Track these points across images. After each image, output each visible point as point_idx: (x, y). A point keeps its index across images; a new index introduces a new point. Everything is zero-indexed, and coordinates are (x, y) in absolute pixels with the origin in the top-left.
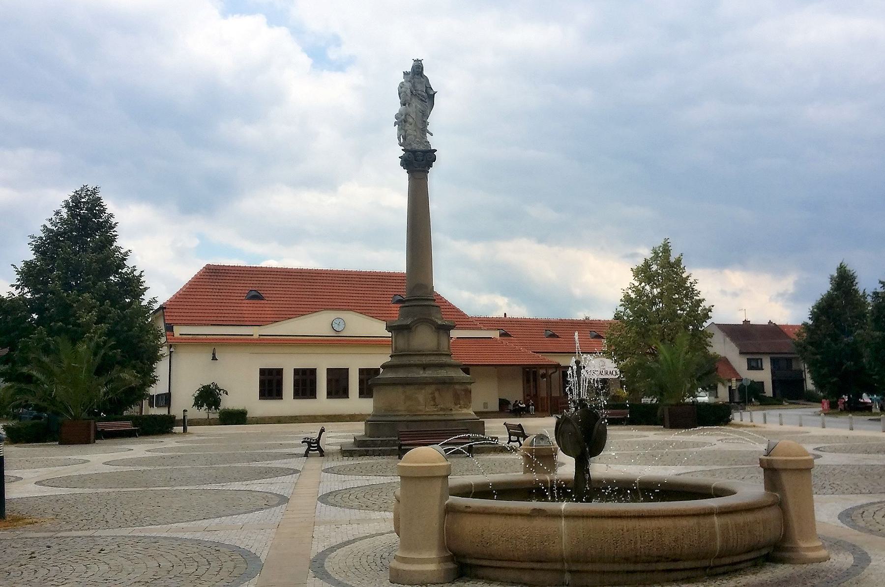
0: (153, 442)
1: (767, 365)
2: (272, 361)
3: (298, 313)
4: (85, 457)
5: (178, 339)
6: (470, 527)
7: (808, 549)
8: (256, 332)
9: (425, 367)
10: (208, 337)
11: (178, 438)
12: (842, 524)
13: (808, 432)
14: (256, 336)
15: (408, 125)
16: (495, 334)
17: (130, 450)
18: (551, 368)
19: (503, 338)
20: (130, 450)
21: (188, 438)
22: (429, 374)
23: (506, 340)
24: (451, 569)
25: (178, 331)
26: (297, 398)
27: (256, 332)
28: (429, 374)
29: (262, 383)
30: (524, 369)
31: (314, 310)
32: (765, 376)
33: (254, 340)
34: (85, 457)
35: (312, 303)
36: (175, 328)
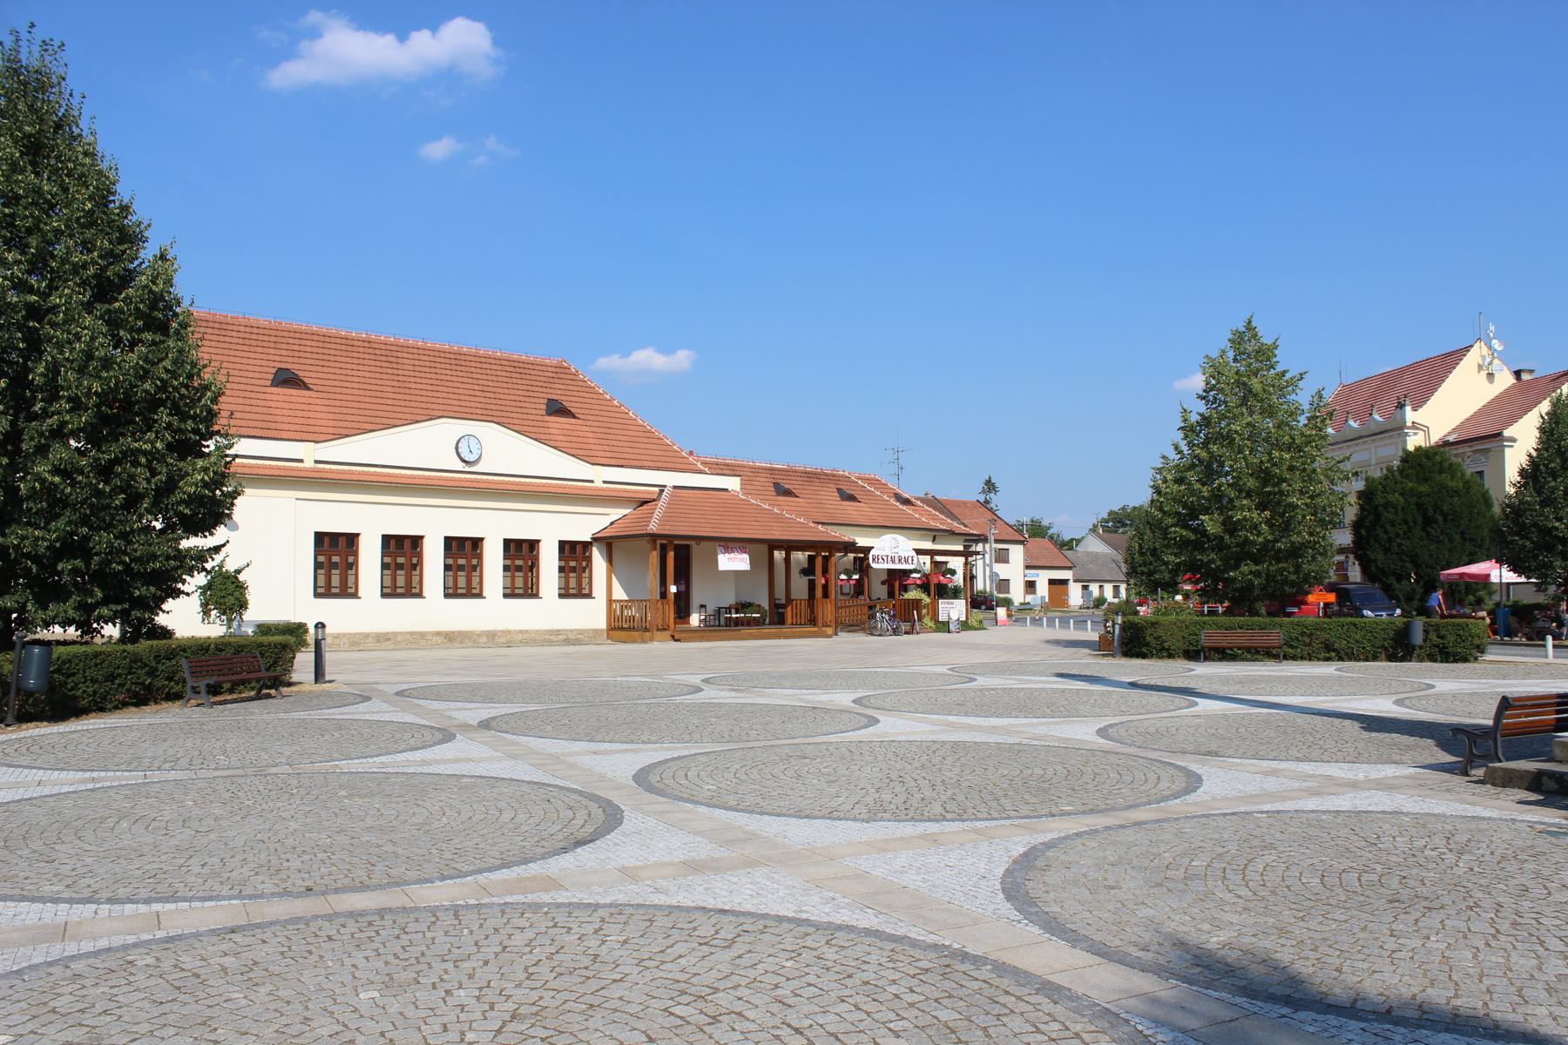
8: (308, 453)
14: (309, 464)
27: (308, 453)
33: (306, 470)
36: (601, 623)
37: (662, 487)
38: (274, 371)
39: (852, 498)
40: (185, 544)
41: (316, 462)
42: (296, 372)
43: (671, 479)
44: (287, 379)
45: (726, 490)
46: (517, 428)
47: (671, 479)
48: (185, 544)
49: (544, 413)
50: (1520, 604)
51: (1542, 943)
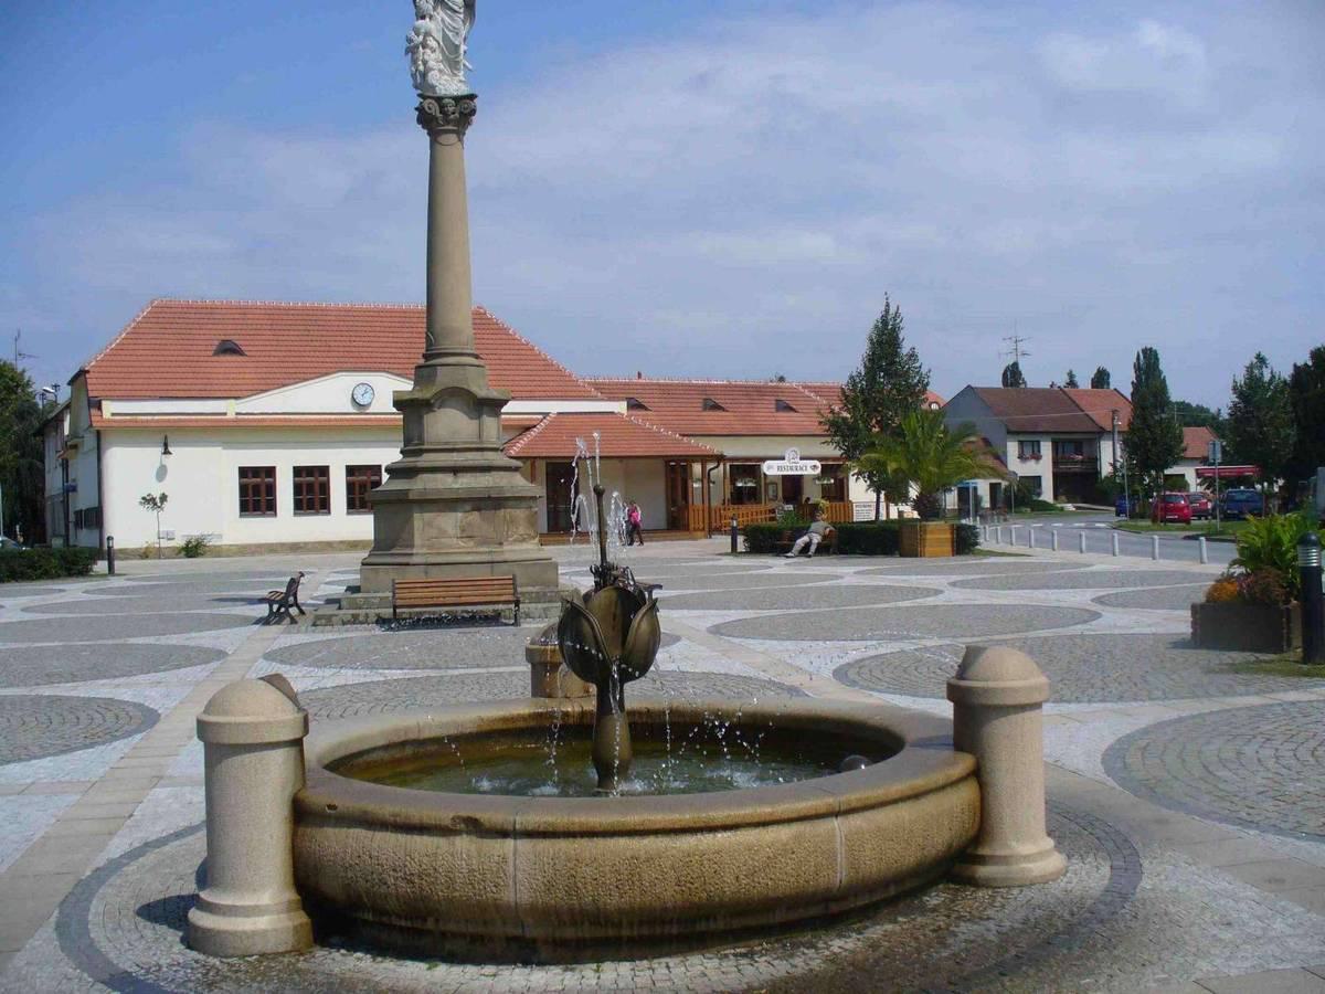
0: (37, 593)
1: (1046, 449)
2: (257, 457)
3: (320, 370)
4: (61, 587)
5: (109, 421)
6: (338, 844)
7: (1027, 858)
8: (230, 408)
9: (455, 470)
10: (156, 418)
11: (102, 584)
12: (1105, 776)
13: (1088, 566)
14: (231, 416)
15: (428, 51)
16: (620, 407)
17: (60, 591)
18: (711, 461)
19: (634, 412)
20: (60, 591)
21: (115, 582)
22: (465, 482)
23: (638, 417)
24: (301, 925)
25: (109, 408)
26: (300, 515)
27: (230, 408)
28: (465, 482)
29: (243, 489)
30: (667, 462)
31: (306, 376)
32: (1043, 468)
33: (228, 421)
34: (61, 587)
35: (297, 359)
36: (105, 404)
37: (546, 414)
38: (217, 343)
39: (790, 409)
40: (66, 432)
41: (237, 414)
42: (237, 342)
43: (554, 407)
44: (229, 349)
45: (612, 413)
46: (396, 371)
47: (554, 407)
48: (66, 432)
49: (773, 410)
50: (1282, 366)
51: (1107, 833)
